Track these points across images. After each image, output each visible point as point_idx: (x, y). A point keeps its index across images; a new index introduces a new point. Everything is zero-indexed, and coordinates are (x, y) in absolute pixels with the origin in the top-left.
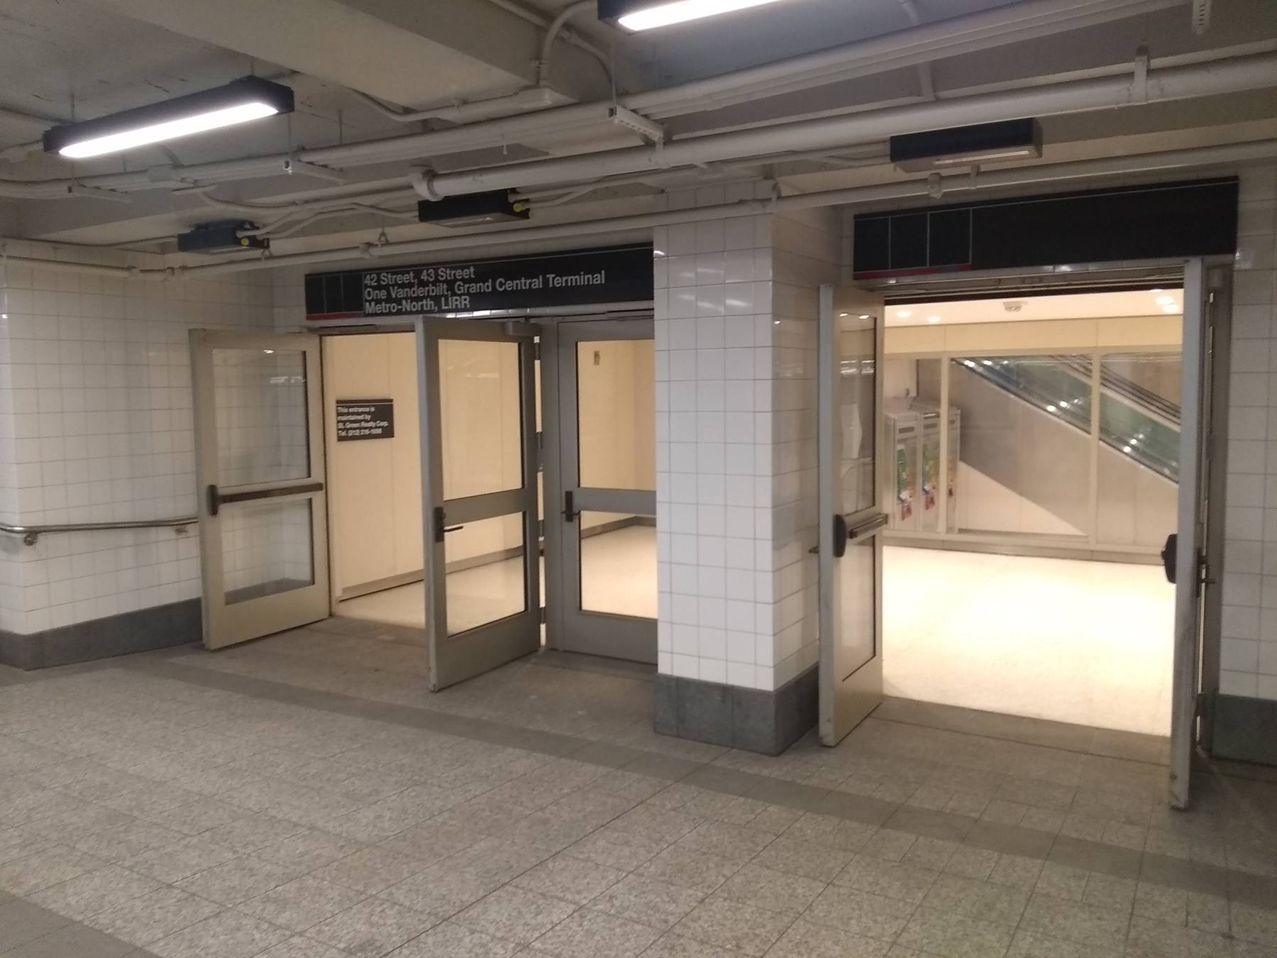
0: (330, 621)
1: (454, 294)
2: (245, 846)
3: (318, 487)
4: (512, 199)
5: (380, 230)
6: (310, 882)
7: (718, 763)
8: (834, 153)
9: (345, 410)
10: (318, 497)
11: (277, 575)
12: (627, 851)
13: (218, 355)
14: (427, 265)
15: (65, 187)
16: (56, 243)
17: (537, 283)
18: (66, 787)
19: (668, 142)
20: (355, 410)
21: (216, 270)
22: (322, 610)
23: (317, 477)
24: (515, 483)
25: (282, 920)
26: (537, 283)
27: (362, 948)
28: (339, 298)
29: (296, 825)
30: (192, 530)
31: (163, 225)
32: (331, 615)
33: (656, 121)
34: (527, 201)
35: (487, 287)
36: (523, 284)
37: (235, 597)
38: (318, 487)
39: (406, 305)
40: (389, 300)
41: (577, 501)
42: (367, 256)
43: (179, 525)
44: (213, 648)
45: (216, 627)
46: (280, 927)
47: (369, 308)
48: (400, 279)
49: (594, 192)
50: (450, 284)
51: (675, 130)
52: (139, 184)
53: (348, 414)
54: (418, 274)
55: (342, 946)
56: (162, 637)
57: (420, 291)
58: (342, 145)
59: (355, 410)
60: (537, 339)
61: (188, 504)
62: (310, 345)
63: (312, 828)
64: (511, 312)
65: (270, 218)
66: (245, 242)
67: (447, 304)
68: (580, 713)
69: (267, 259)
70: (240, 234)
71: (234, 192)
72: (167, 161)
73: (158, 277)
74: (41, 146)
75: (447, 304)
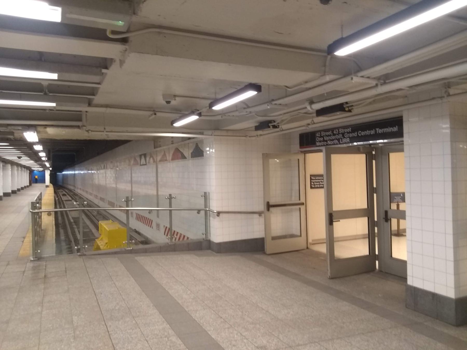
0: (307, 250)
1: (344, 137)
2: (246, 312)
3: (303, 204)
4: (345, 106)
5: (311, 120)
6: (258, 326)
7: (426, 324)
8: (462, 77)
9: (314, 178)
10: (303, 208)
11: (290, 233)
12: (366, 343)
13: (271, 161)
14: (335, 128)
15: (220, 116)
16: (228, 130)
17: (373, 132)
18: (210, 286)
19: (385, 83)
20: (318, 178)
21: (269, 135)
22: (304, 246)
23: (302, 200)
24: (364, 205)
25: (244, 334)
26: (373, 132)
27: (261, 347)
28: (308, 141)
29: (263, 309)
30: (263, 215)
31: (251, 124)
32: (307, 248)
33: (372, 78)
34: (352, 106)
35: (355, 134)
36: (368, 132)
37: (274, 238)
38: (303, 204)
39: (329, 142)
40: (324, 141)
41: (390, 214)
42: (307, 128)
43: (260, 213)
44: (268, 253)
45: (269, 247)
46: (243, 336)
47: (318, 144)
48: (327, 133)
49: (374, 101)
50: (343, 134)
51: (385, 79)
52: (237, 114)
53: (316, 179)
54: (333, 132)
55: (256, 345)
56: (252, 248)
57: (333, 137)
58: (286, 96)
59: (318, 178)
60: (374, 153)
61: (261, 207)
62: (301, 157)
63: (267, 311)
64: (361, 143)
65: (278, 119)
66: (271, 127)
67: (342, 141)
68: (380, 295)
69: (281, 131)
70: (270, 125)
71: (265, 113)
72: (245, 106)
73: (254, 138)
74: (208, 108)
75: (342, 141)
